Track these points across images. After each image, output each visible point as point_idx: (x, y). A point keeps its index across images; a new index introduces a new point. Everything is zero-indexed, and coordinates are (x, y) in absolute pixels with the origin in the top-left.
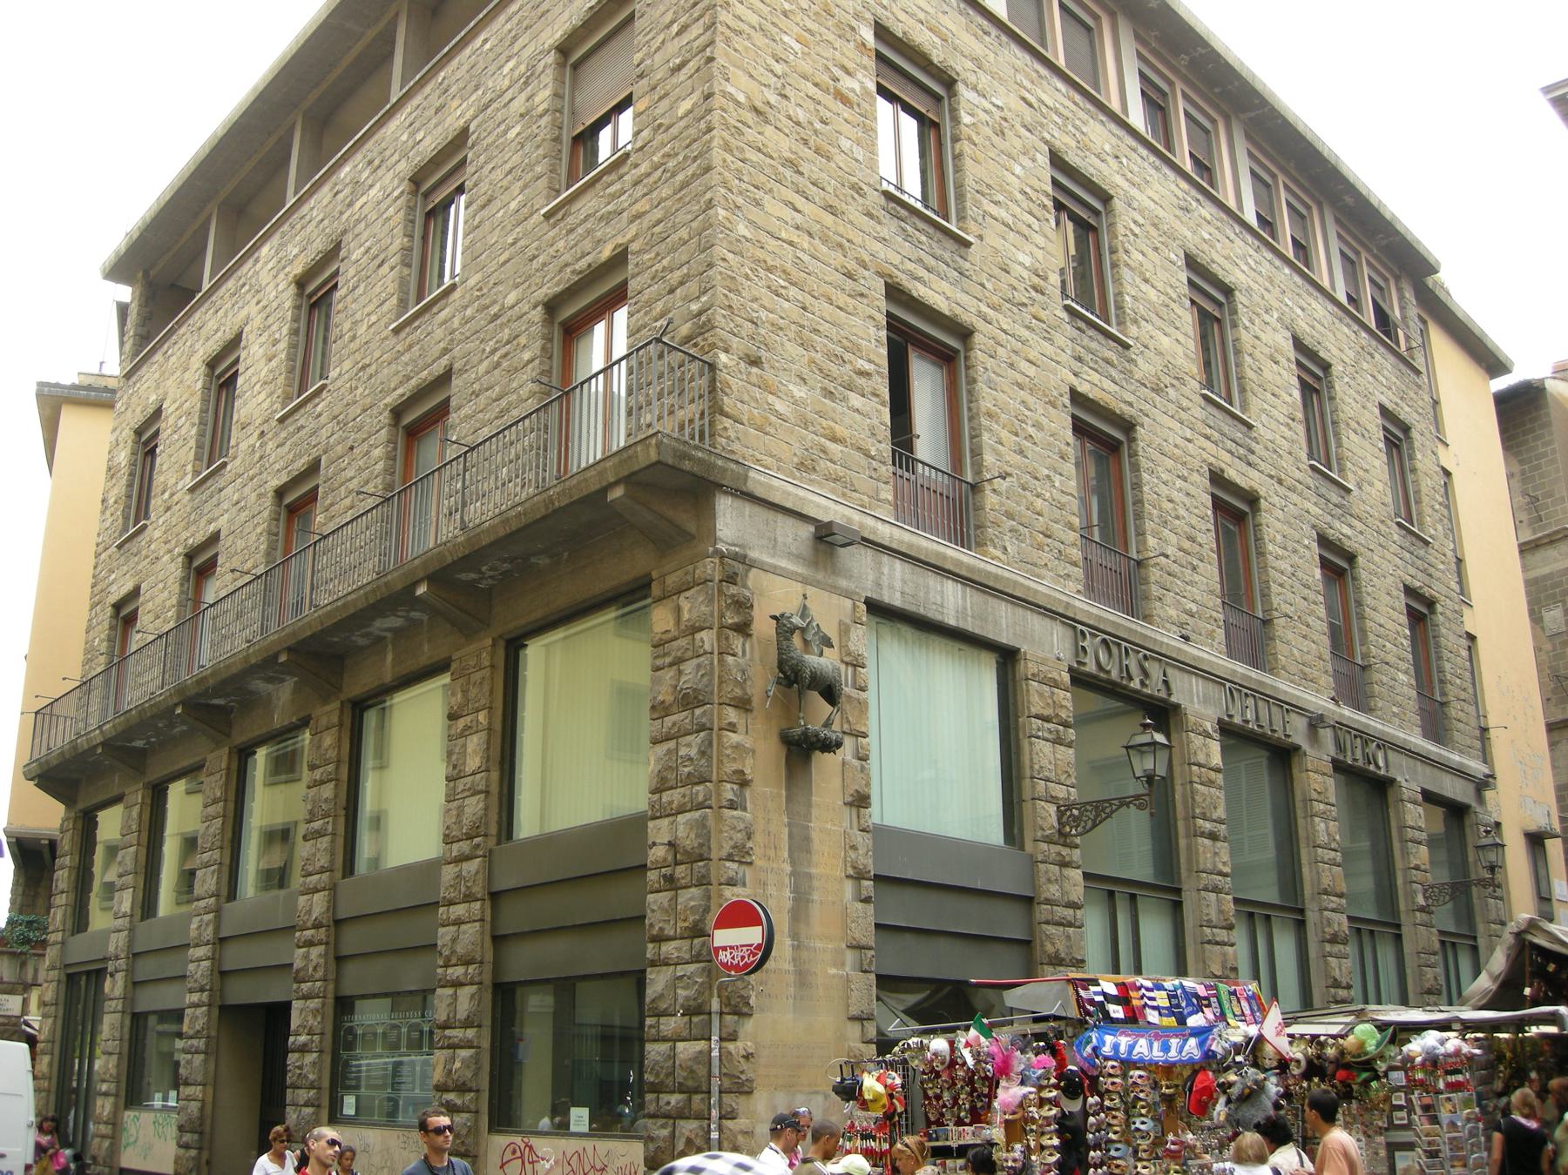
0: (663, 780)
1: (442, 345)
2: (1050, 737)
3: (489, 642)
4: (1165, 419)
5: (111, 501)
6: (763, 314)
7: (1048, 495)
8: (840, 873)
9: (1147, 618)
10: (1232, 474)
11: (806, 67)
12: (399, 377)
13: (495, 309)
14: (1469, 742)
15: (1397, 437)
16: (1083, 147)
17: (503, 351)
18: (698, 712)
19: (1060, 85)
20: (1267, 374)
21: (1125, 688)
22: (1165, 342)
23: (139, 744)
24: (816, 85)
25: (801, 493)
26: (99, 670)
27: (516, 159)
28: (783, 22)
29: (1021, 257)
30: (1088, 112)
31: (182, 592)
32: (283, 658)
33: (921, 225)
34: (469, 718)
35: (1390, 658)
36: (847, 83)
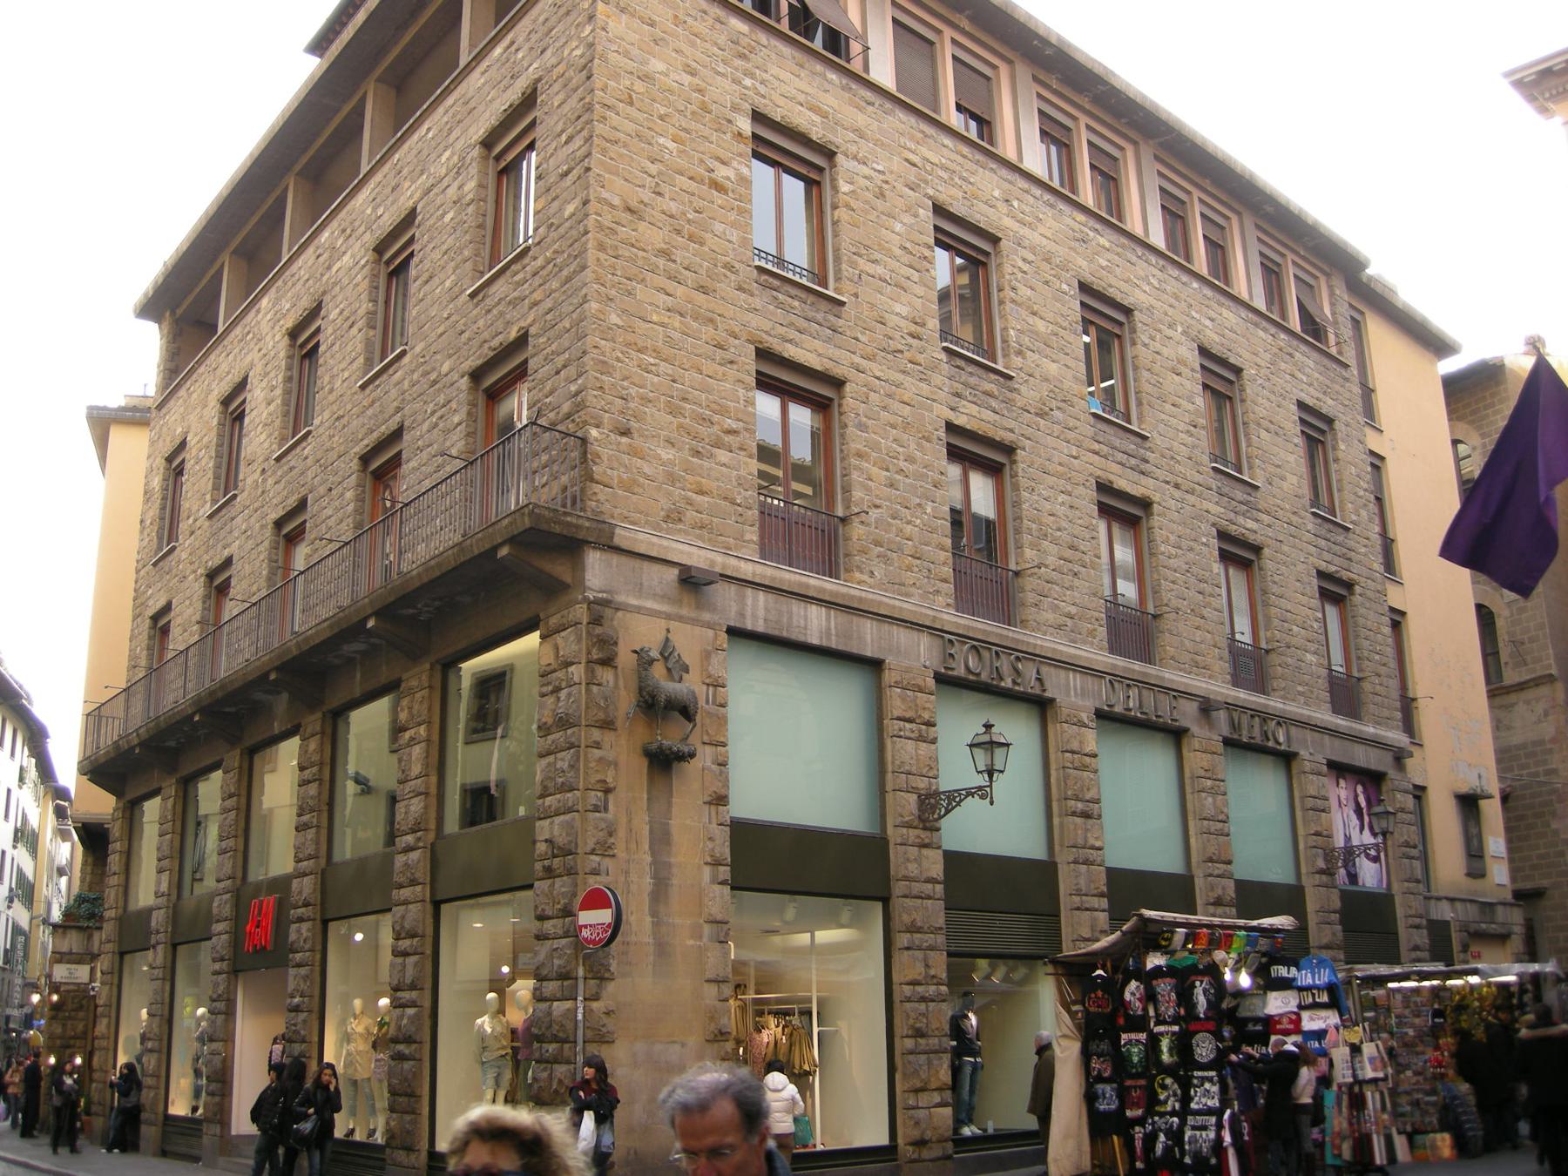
0: (545, 788)
3: (427, 666)
6: (633, 391)
10: (1121, 484)
11: (682, 162)
12: (364, 430)
13: (433, 376)
14: (1386, 713)
15: (1317, 430)
19: (948, 141)
21: (997, 686)
22: (1053, 369)
23: (172, 744)
24: (691, 178)
27: (450, 241)
29: (898, 308)
30: (977, 163)
32: (273, 676)
33: (794, 291)
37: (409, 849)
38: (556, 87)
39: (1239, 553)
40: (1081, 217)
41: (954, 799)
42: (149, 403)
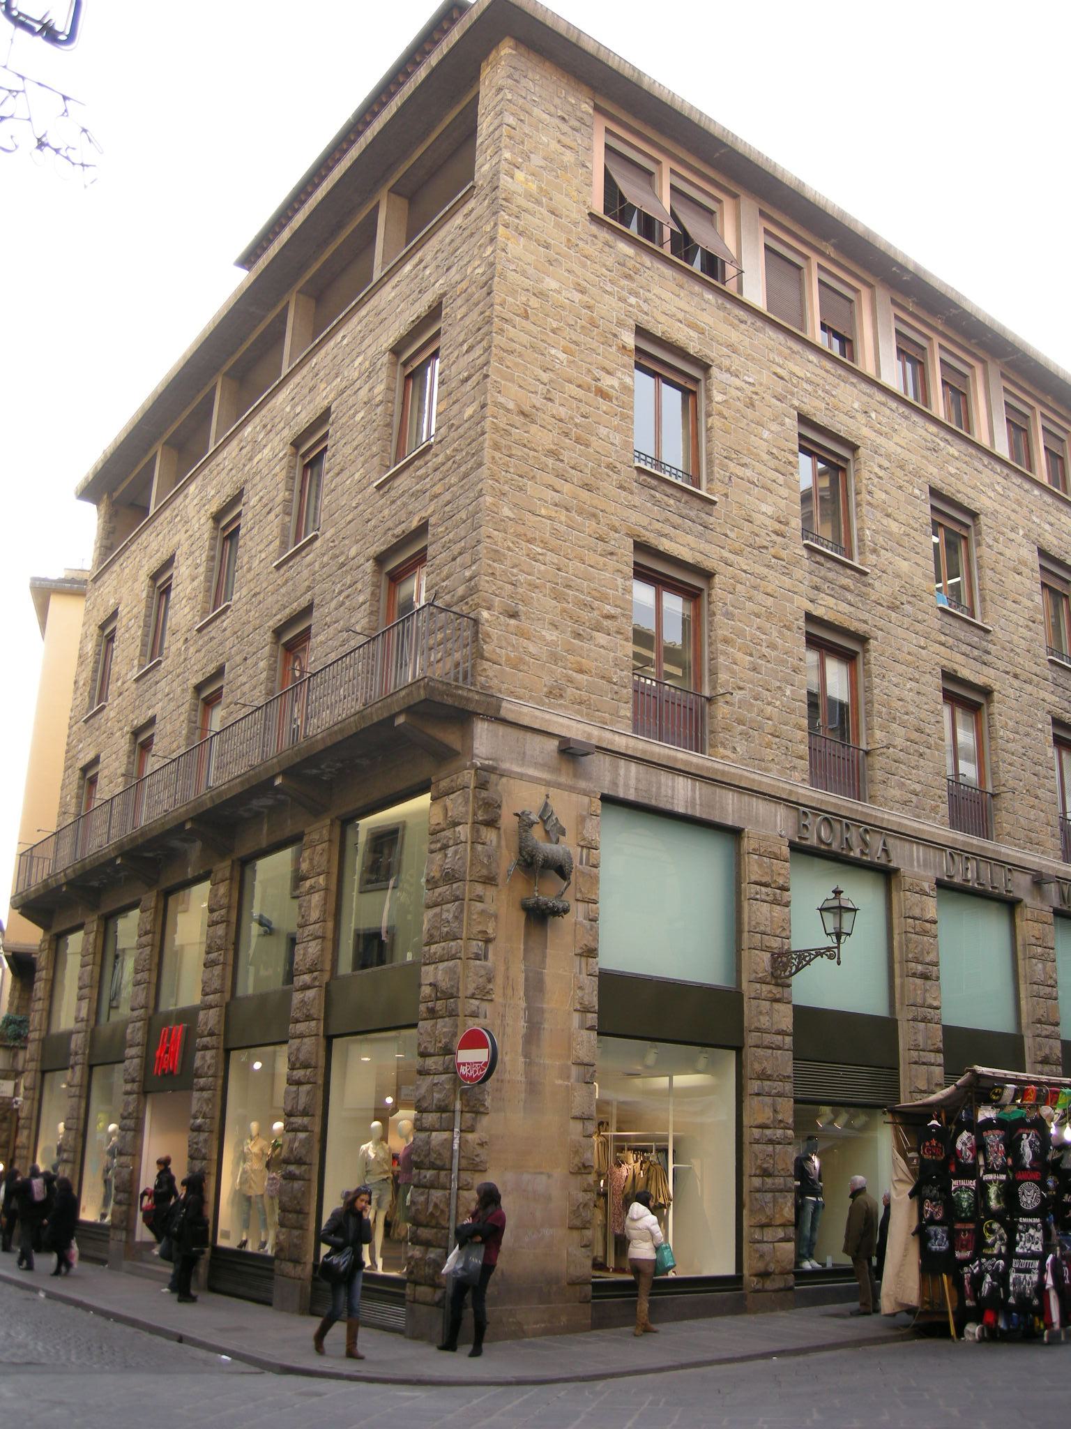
1: (307, 583)
2: (768, 899)
3: (328, 822)
5: (81, 683)
6: (522, 577)
7: (778, 703)
9: (872, 799)
10: (965, 673)
11: (573, 373)
12: (277, 607)
13: (342, 559)
17: (345, 594)
18: (455, 886)
19: (813, 357)
21: (846, 856)
23: (95, 884)
24: (579, 386)
25: (547, 716)
26: (70, 821)
27: (360, 438)
30: (839, 377)
31: (129, 763)
32: (188, 826)
33: (670, 491)
34: (313, 880)
37: (306, 987)
38: (459, 302)
41: (805, 958)
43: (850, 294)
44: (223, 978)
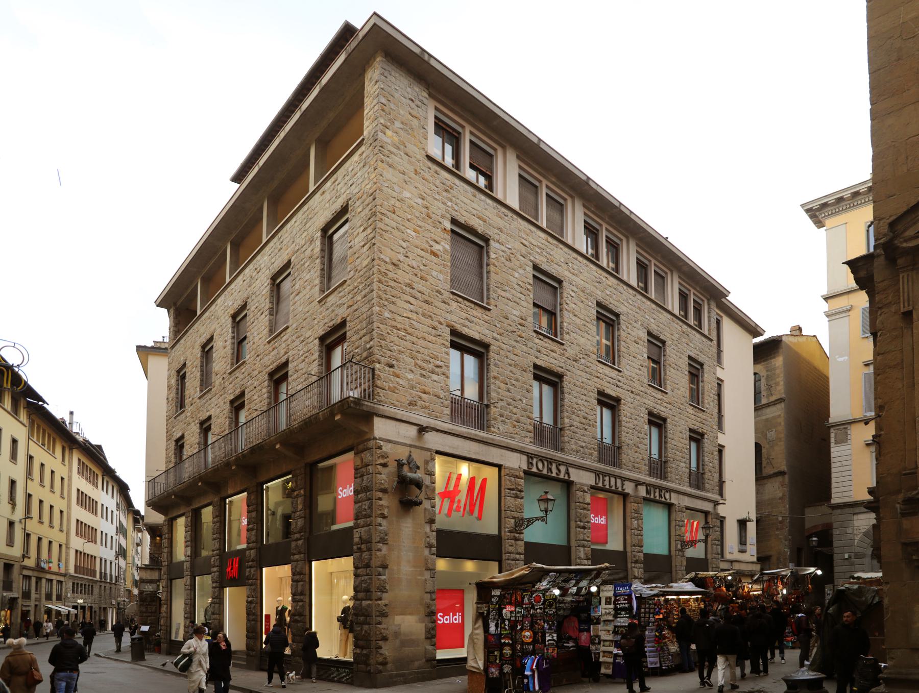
4: (579, 373)
6: (396, 348)
8: (423, 545)
9: (562, 450)
11: (417, 242)
13: (302, 338)
15: (696, 370)
16: (550, 261)
20: (632, 349)
28: (407, 224)
29: (515, 312)
35: (679, 458)
36: (436, 247)
37: (297, 540)
38: (358, 203)
39: (657, 421)
40: (600, 271)
41: (530, 521)
42: (167, 345)
43: (562, 201)
44: (256, 536)
